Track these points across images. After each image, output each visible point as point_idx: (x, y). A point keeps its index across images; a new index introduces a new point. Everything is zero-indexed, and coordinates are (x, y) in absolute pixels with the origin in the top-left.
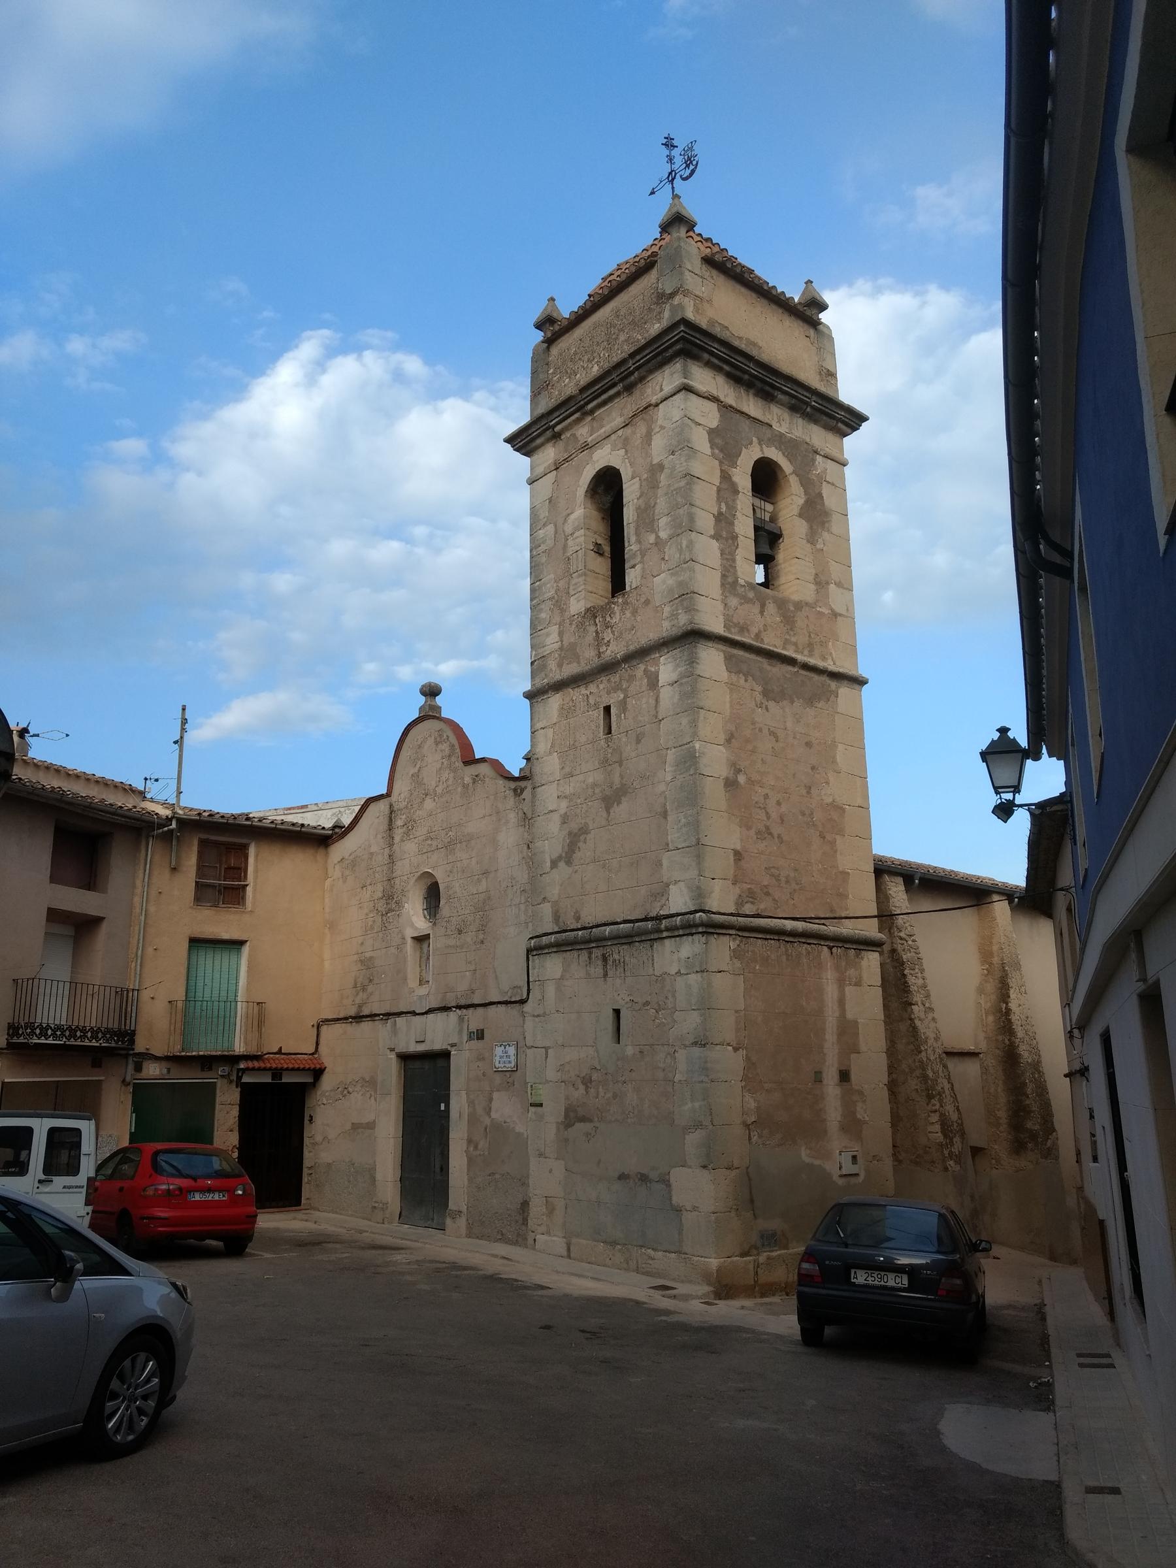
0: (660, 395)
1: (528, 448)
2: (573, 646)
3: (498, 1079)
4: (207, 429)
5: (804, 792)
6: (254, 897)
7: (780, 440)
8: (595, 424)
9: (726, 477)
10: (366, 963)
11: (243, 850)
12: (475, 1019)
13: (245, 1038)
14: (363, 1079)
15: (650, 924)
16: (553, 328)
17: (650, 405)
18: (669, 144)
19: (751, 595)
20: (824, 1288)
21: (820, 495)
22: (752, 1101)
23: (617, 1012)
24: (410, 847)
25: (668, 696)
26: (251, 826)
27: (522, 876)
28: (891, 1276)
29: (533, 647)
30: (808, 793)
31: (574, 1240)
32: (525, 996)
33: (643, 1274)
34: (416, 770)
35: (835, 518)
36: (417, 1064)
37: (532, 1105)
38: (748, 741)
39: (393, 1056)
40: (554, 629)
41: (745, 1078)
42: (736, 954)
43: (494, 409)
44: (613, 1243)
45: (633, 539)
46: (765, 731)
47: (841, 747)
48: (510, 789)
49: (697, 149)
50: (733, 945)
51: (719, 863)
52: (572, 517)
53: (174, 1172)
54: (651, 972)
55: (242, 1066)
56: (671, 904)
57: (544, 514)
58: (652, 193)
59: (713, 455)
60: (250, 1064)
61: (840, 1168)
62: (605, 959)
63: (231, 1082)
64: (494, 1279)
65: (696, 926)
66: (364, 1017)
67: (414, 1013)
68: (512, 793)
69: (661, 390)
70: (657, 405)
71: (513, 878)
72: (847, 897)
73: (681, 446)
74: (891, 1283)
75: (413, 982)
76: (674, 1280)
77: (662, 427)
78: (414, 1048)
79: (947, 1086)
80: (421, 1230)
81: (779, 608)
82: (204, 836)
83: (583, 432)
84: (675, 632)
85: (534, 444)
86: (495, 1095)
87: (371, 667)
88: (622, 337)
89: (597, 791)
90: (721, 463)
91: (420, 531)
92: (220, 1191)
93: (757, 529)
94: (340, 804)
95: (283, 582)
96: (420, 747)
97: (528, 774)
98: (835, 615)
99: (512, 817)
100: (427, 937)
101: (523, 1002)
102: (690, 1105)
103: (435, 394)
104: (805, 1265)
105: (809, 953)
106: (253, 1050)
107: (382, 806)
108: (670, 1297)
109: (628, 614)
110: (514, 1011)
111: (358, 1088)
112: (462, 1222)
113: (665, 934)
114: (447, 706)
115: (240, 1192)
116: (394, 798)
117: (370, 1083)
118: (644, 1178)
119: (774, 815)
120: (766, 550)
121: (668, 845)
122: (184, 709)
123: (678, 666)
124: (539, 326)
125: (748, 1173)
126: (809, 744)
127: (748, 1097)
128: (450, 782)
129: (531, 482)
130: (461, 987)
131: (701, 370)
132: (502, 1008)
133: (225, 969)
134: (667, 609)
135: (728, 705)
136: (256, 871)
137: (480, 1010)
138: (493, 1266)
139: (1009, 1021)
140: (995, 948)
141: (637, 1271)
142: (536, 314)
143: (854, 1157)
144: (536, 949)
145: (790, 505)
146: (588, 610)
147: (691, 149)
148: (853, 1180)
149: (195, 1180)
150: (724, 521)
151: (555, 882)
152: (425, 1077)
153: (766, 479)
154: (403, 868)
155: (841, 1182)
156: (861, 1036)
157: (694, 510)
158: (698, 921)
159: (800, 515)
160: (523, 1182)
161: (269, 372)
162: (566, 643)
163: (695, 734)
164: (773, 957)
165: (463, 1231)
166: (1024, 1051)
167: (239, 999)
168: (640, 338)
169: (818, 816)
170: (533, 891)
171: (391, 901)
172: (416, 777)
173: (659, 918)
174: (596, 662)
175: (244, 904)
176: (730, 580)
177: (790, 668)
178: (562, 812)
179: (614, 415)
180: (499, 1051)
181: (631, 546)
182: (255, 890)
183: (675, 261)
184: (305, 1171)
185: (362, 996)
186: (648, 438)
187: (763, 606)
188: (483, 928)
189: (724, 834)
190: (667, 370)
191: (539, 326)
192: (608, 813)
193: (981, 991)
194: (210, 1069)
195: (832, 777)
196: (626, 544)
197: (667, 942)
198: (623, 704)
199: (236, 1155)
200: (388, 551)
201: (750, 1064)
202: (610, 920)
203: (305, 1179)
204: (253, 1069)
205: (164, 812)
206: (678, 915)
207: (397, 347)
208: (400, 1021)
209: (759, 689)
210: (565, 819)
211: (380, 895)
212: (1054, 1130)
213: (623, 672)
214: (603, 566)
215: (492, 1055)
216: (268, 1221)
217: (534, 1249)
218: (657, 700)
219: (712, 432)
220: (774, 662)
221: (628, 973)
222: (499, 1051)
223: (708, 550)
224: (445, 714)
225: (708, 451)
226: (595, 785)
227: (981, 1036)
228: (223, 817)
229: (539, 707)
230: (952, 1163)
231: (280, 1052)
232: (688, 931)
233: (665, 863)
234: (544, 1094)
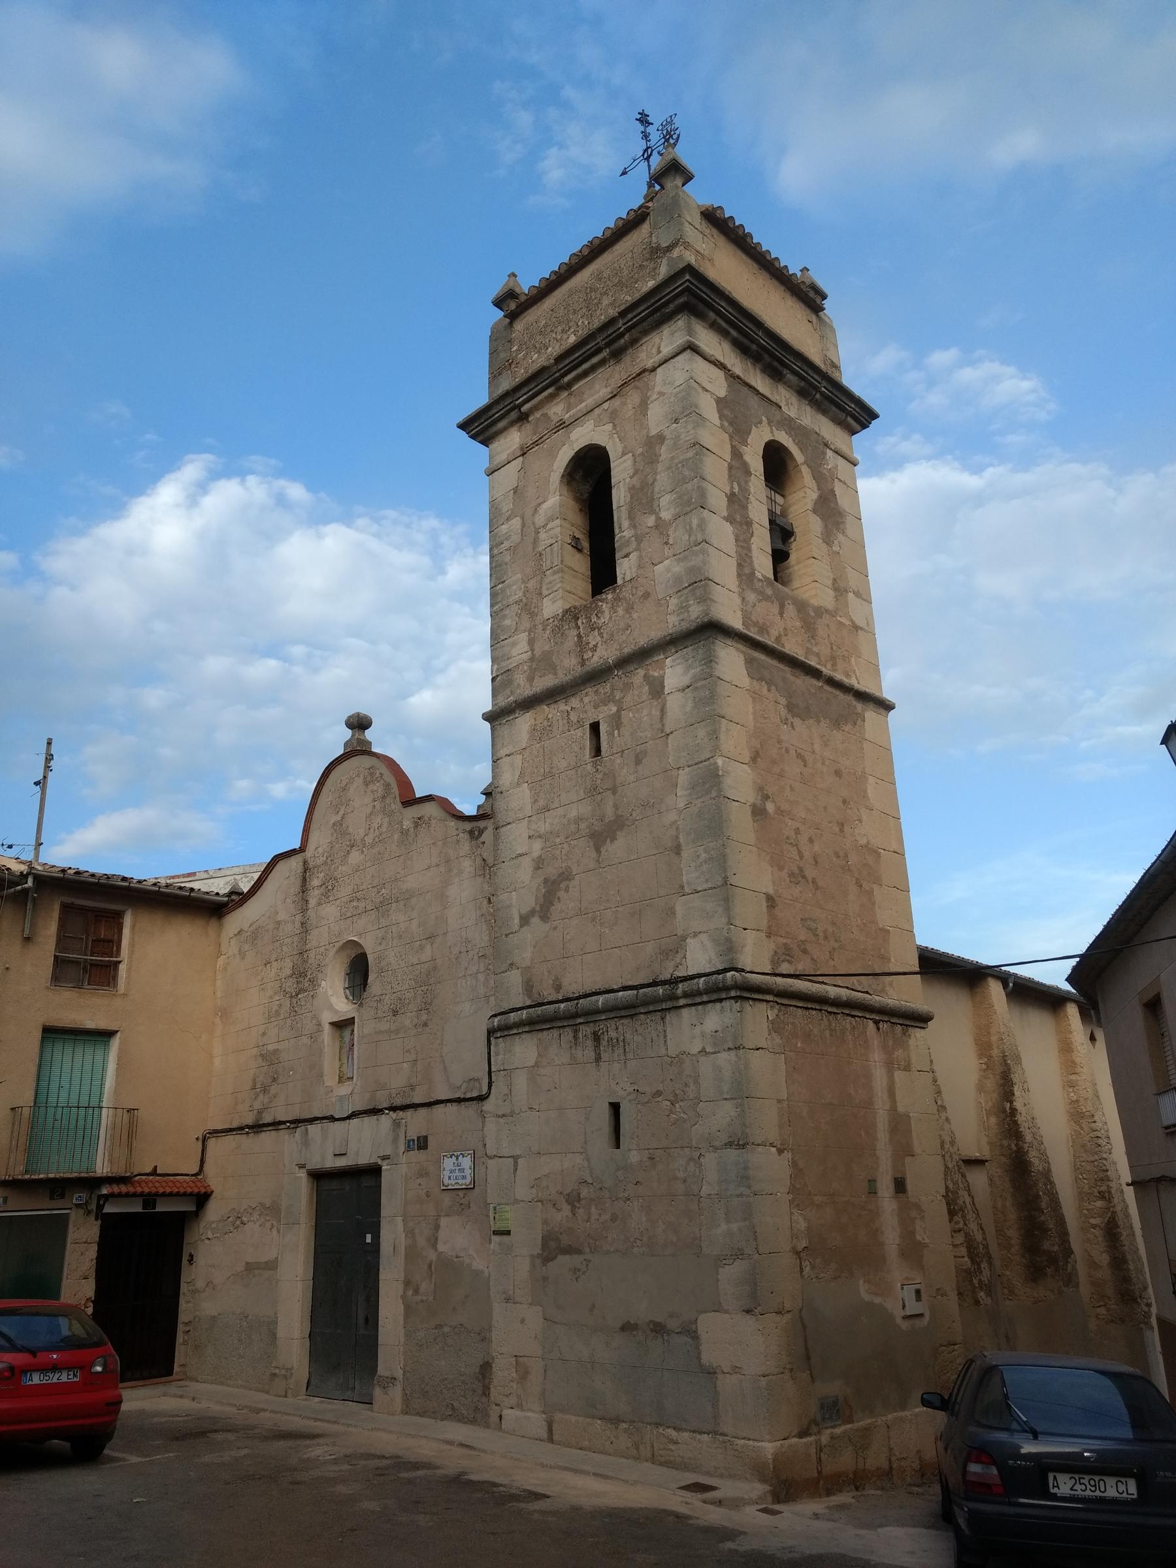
0: (658, 358)
1: (487, 434)
2: (547, 656)
3: (447, 1200)
4: (82, 545)
5: (837, 829)
6: (128, 977)
7: (789, 424)
8: (572, 400)
9: (736, 454)
10: (269, 1058)
11: (116, 919)
12: (415, 1123)
13: (111, 1155)
15: (660, 990)
16: (514, 304)
17: (644, 371)
18: (644, 119)
19: (769, 592)
20: (1010, 1504)
21: (833, 492)
22: (801, 1219)
23: (615, 1108)
24: (330, 911)
25: (677, 706)
26: (128, 889)
27: (480, 937)
28: (1111, 1481)
29: (494, 660)
30: (842, 830)
31: (558, 1416)
32: (485, 1090)
33: (661, 1464)
34: (339, 818)
35: (849, 520)
36: (334, 1184)
37: (496, 1233)
38: (774, 762)
39: (302, 1174)
40: (523, 637)
41: (792, 1190)
42: (775, 1027)
43: (376, 535)
44: (615, 1421)
45: (626, 524)
46: (792, 752)
47: (871, 780)
48: (464, 831)
49: (677, 122)
50: (772, 1014)
51: (750, 910)
52: (544, 506)
53: (7, 1345)
54: (663, 1052)
55: (105, 1191)
56: (690, 963)
57: (507, 506)
58: (624, 173)
59: (722, 427)
60: (116, 1189)
61: (904, 1307)
62: (597, 1038)
63: (89, 1212)
64: (459, 1482)
65: (727, 989)
67: (332, 1119)
68: (467, 836)
69: (659, 352)
70: (654, 369)
71: (467, 941)
72: (889, 960)
73: (686, 411)
74: (1111, 1493)
75: (330, 1080)
76: (708, 1474)
77: (661, 394)
78: (332, 1163)
79: (968, 1200)
80: (338, 1405)
81: (799, 611)
82: (68, 900)
83: (557, 410)
84: (685, 626)
85: (494, 429)
86: (444, 1221)
87: (243, 784)
88: (606, 301)
89: (583, 826)
90: (731, 437)
91: (298, 651)
92: (69, 1368)
93: (771, 522)
94: (236, 870)
95: (154, 698)
96: (344, 789)
97: (488, 811)
98: (856, 628)
99: (467, 865)
100: (351, 1021)
101: (481, 1098)
102: (724, 1227)
103: (317, 519)
104: (974, 1468)
105: (854, 1028)
106: (119, 1170)
107: (295, 863)
108: (713, 1503)
109: (621, 612)
110: (469, 1111)
111: (255, 1216)
112: (397, 1392)
113: (682, 1002)
114: (379, 739)
115: (99, 1369)
116: (309, 853)
117: (272, 1211)
118: (658, 1329)
119: (807, 854)
120: (780, 546)
121: (682, 887)
122: (49, 743)
123: (689, 668)
124: (498, 303)
125: (800, 1316)
126: (838, 773)
127: (797, 1216)
128: (384, 829)
129: (490, 473)
131: (706, 331)
132: (452, 1108)
133: (88, 1067)
134: (674, 602)
135: (751, 717)
136: (132, 945)
137: (423, 1111)
138: (452, 1462)
139: (1016, 1123)
140: (994, 1038)
141: (653, 1459)
142: (496, 289)
143: (918, 1292)
144: (500, 1029)
145: (802, 501)
146: (566, 612)
147: (671, 123)
148: (918, 1323)
149: (33, 1353)
150: (737, 503)
151: (525, 945)
152: (346, 1202)
153: (777, 466)
154: (319, 938)
155: (905, 1325)
156: (914, 1134)
157: (705, 484)
158: (729, 982)
159: (815, 511)
160: (484, 1338)
161: (149, 491)
162: (538, 652)
163: (716, 749)
164: (816, 1031)
166: (1033, 1156)
167: (104, 1104)
168: (628, 298)
169: (853, 859)
170: (496, 955)
171: (303, 979)
172: (339, 828)
173: (674, 981)
174: (579, 671)
175: (115, 985)
176: (747, 571)
177: (814, 682)
178: (536, 854)
179: (597, 387)
180: (448, 1163)
181: (623, 529)
182: (129, 969)
183: (673, 211)
184: (181, 1328)
186: (643, 407)
187: (782, 607)
188: (426, 1007)
189: (754, 875)
190: (666, 330)
191: (498, 303)
192: (598, 851)
193: (980, 1088)
194: (62, 1196)
195: (864, 814)
196: (617, 531)
197: (685, 1012)
198: (616, 721)
199: (90, 1311)
200: (264, 670)
201: (797, 1171)
202: (607, 987)
203: (180, 1339)
204: (120, 1195)
205: (17, 868)
206: (699, 976)
207: (279, 474)
208: (312, 1128)
209: (783, 701)
210: (539, 864)
211: (289, 972)
212: (1072, 1252)
213: (617, 680)
214: (581, 564)
215: (439, 1168)
216: (139, 1400)
217: (500, 1429)
218: (663, 711)
219: (719, 401)
220: (798, 672)
221: (630, 1055)
223: (722, 533)
224: (375, 749)
225: (718, 422)
226: (579, 820)
227: (984, 1140)
228: (93, 875)
229: (504, 731)
230: (982, 1294)
231: (154, 1172)
232: (715, 996)
233: (680, 911)
234: (511, 1217)
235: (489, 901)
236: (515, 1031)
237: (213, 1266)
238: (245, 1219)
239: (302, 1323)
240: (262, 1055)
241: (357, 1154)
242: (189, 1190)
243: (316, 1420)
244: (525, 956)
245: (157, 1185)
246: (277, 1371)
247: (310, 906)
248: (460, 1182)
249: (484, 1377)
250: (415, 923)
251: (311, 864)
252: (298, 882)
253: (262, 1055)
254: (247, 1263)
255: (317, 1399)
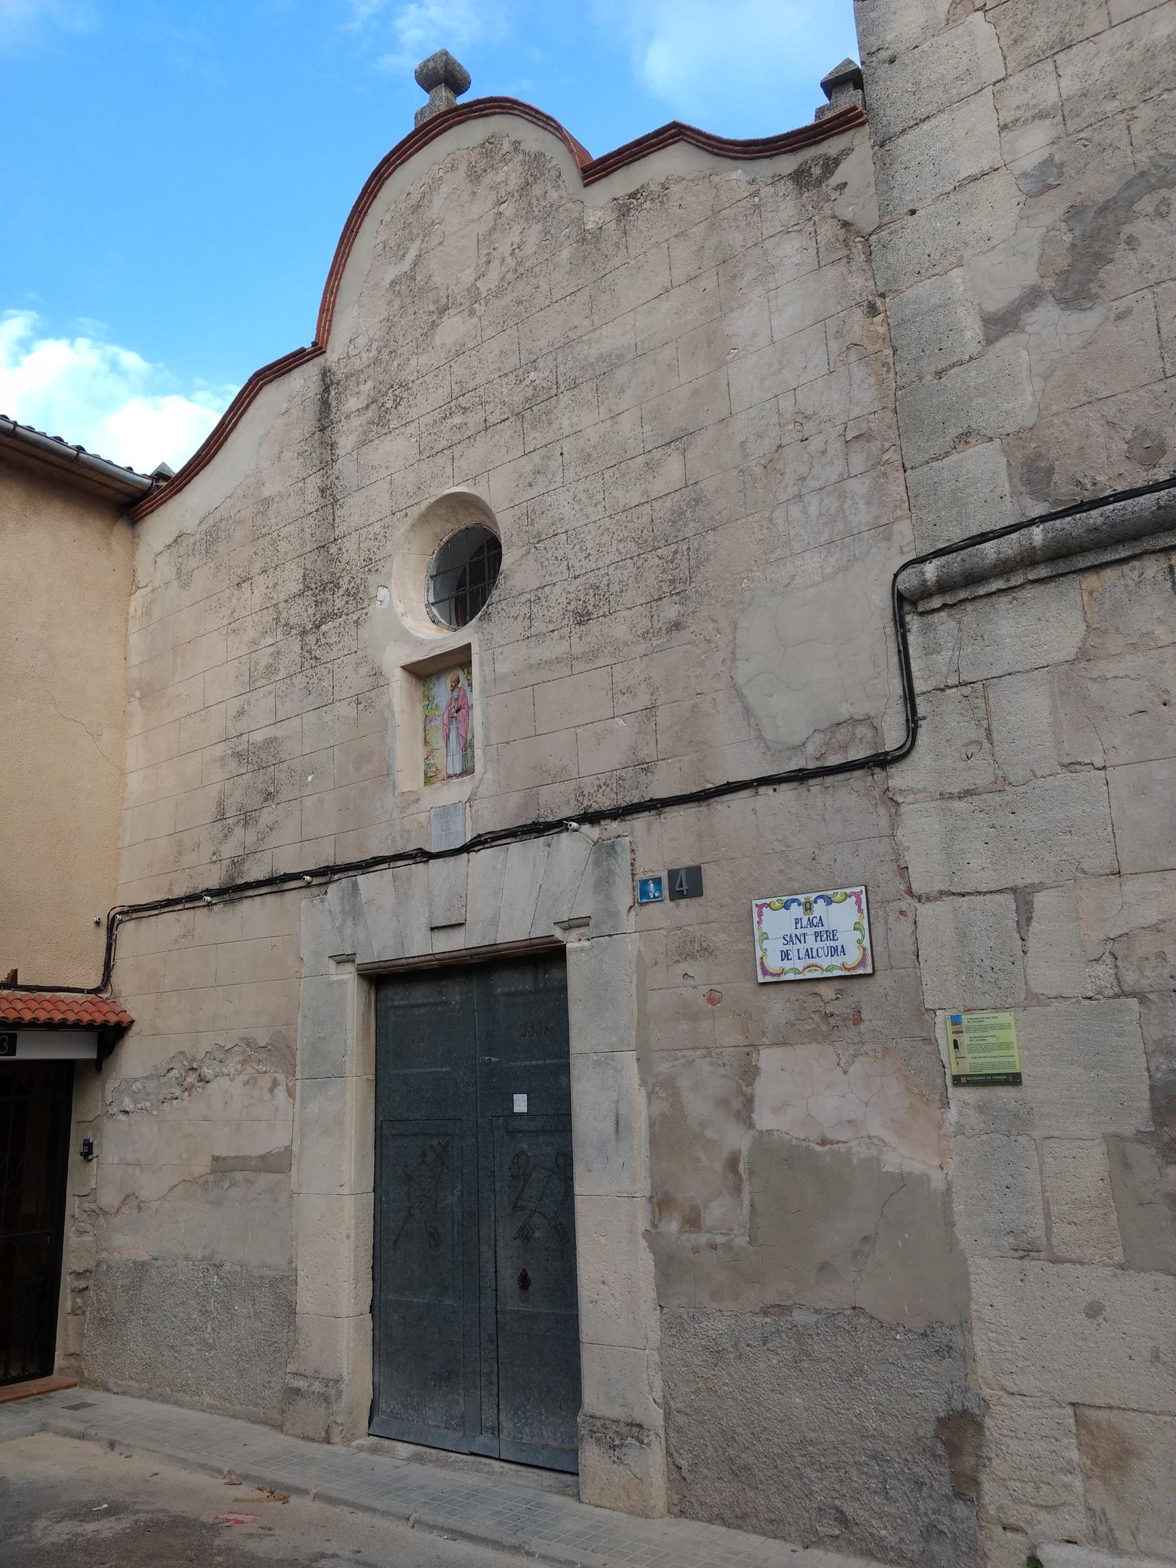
12: (659, 844)
14: (248, 1042)
24: (394, 449)
27: (856, 395)
34: (406, 266)
36: (421, 994)
37: (958, 1081)
39: (348, 976)
66: (248, 886)
67: (424, 856)
71: (802, 418)
75: (408, 779)
78: (420, 945)
86: (767, 1059)
96: (416, 208)
101: (882, 761)
103: (153, 389)
107: (303, 380)
110: (848, 795)
111: (232, 1065)
112: (653, 1461)
116: (333, 355)
117: (274, 1053)
128: (529, 250)
130: (595, 762)
165: (659, 1492)
170: (910, 414)
171: (334, 590)
180: (777, 924)
184: (67, 1283)
185: (242, 837)
203: (66, 1302)
207: (112, 340)
208: (365, 881)
211: (295, 587)
222: (777, 924)
235: (873, 310)
236: (999, 584)
237: (138, 1164)
238: (207, 1072)
239: (356, 1281)
240: (238, 755)
241: (494, 922)
242: (86, 1018)
243: (457, 1534)
244: (1022, 405)
245: (20, 1005)
246: (302, 1384)
247: (340, 452)
248: (825, 962)
249: (954, 1450)
250: (627, 423)
251: (339, 373)
252: (312, 413)
253: (238, 755)
254: (216, 1159)
255: (403, 1450)
